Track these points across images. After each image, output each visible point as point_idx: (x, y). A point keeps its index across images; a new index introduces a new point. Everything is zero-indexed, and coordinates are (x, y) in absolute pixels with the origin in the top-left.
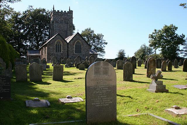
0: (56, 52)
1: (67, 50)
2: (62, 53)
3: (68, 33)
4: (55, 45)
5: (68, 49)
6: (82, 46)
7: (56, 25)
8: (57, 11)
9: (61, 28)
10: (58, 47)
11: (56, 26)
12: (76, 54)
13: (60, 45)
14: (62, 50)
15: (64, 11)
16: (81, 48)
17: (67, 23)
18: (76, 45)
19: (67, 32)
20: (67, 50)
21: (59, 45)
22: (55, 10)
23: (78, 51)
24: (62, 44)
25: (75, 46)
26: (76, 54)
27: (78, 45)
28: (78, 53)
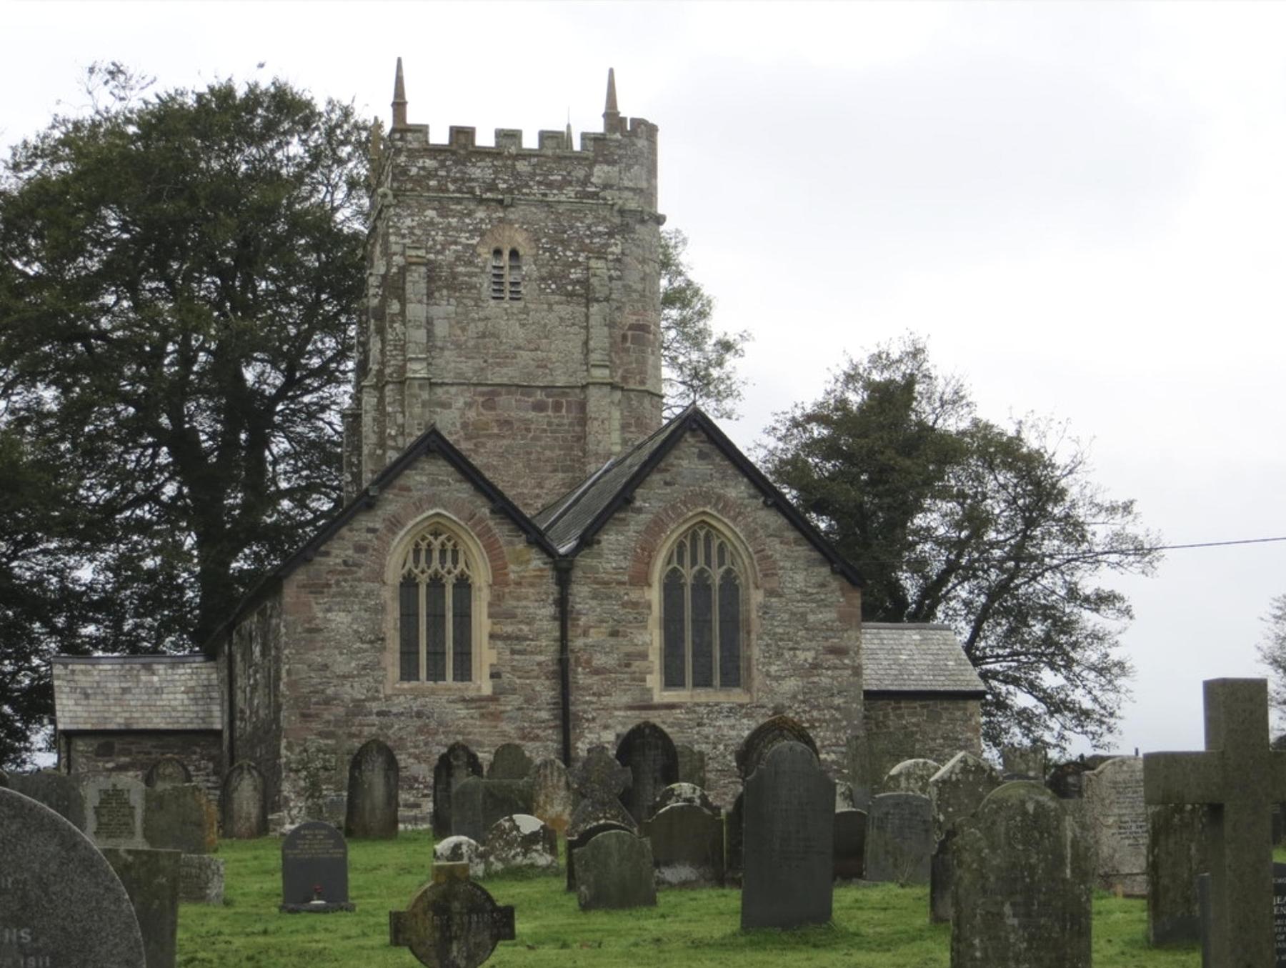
0: (409, 671)
1: (547, 654)
2: (487, 688)
3: (593, 427)
4: (389, 596)
5: (563, 640)
6: (757, 597)
7: (430, 322)
8: (439, 137)
9: (505, 359)
10: (436, 619)
11: (441, 329)
12: (671, 696)
13: (463, 585)
14: (485, 655)
15: (544, 136)
16: (734, 625)
17: (585, 283)
18: (672, 585)
19: (582, 406)
20: (554, 647)
21: (449, 581)
22: (412, 118)
23: (702, 652)
24: (481, 576)
25: (654, 595)
26: (671, 696)
27: (702, 585)
28: (703, 681)
